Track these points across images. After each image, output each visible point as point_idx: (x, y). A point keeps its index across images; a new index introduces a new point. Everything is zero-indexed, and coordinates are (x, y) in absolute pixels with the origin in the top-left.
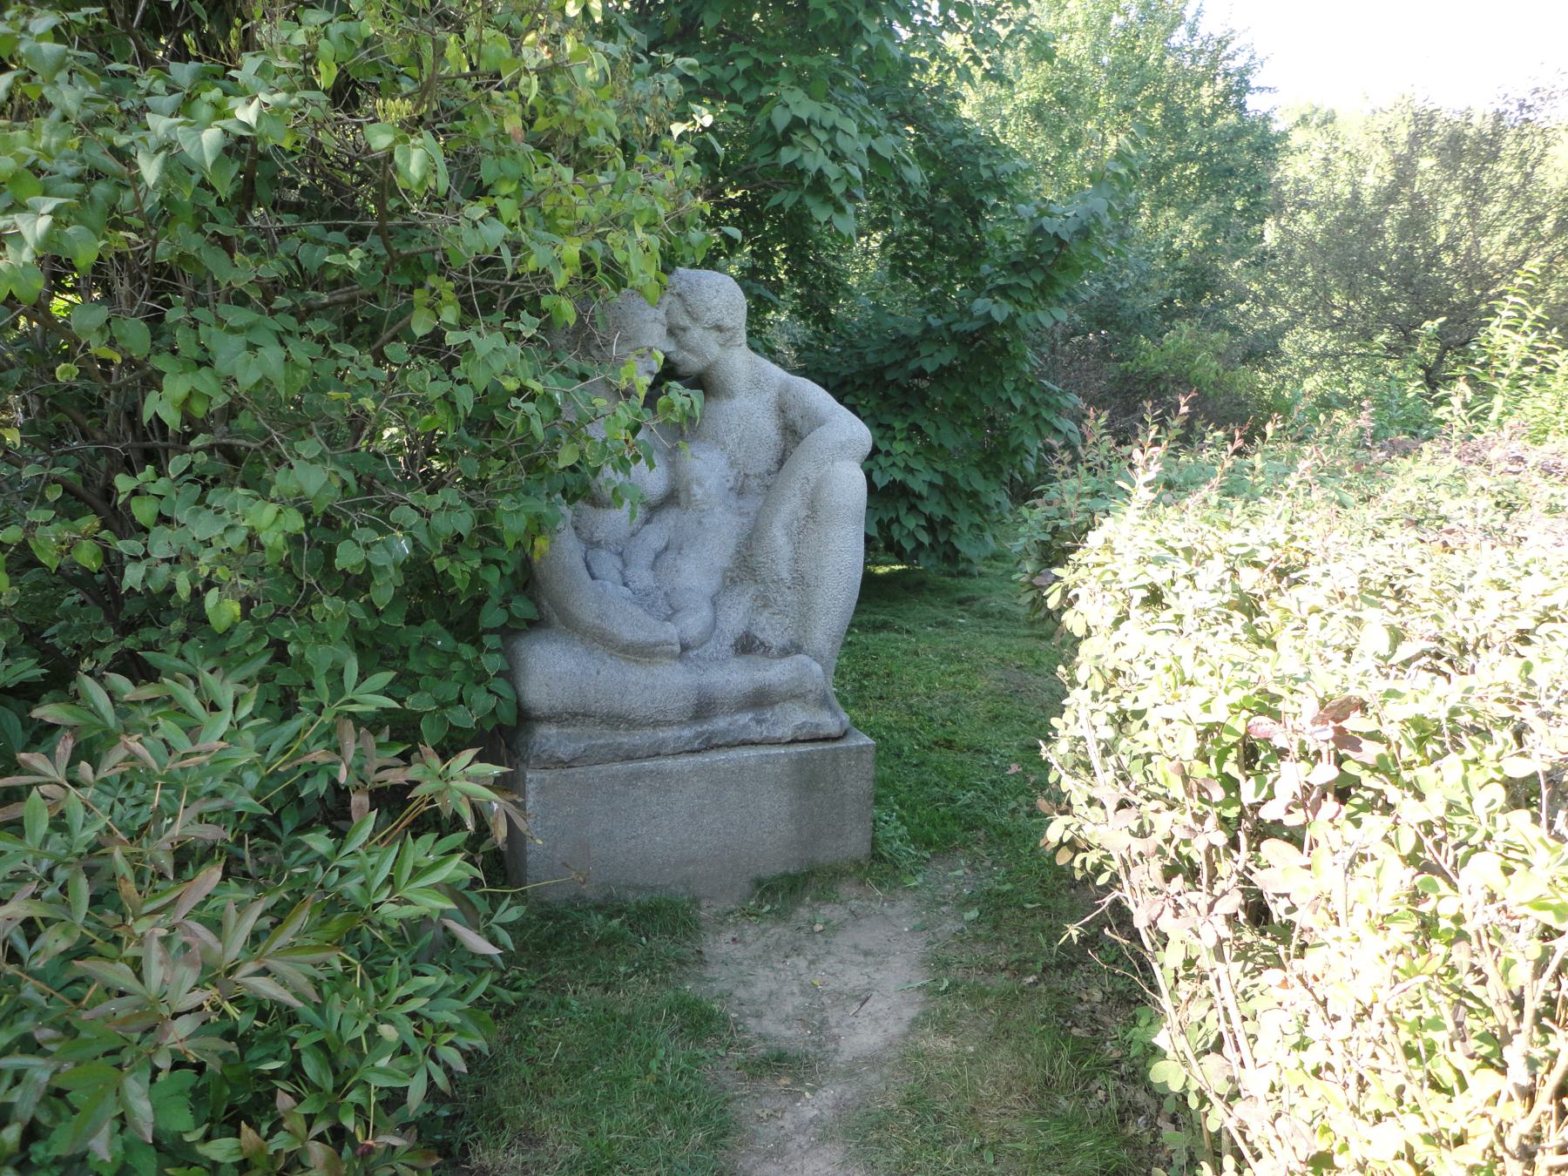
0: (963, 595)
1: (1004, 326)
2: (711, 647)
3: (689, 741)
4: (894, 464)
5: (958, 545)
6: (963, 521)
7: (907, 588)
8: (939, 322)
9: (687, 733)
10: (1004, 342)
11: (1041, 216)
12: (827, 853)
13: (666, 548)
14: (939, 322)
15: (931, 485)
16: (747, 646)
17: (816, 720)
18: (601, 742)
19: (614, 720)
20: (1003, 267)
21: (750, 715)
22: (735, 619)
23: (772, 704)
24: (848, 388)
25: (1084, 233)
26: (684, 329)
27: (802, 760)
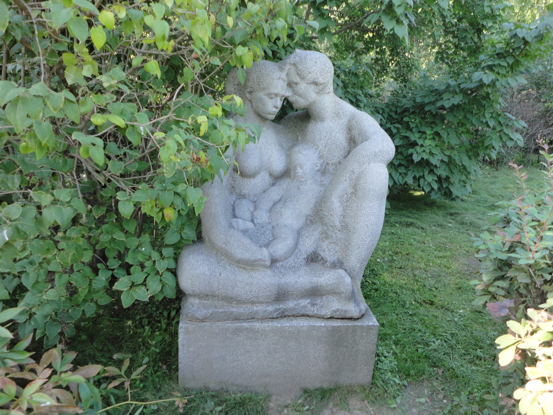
0: (453, 211)
1: (489, 86)
2: (291, 261)
3: (271, 313)
4: (424, 151)
5: (452, 190)
6: (455, 179)
7: (426, 204)
8: (455, 83)
9: (270, 308)
10: (488, 94)
11: (516, 28)
12: (345, 380)
13: (280, 200)
14: (455, 83)
15: (442, 161)
16: (314, 258)
17: (345, 308)
18: (221, 310)
19: (229, 299)
20: (491, 56)
21: (308, 301)
22: (308, 245)
23: (322, 295)
24: (406, 114)
25: (540, 38)
26: (296, 84)
27: (334, 330)
